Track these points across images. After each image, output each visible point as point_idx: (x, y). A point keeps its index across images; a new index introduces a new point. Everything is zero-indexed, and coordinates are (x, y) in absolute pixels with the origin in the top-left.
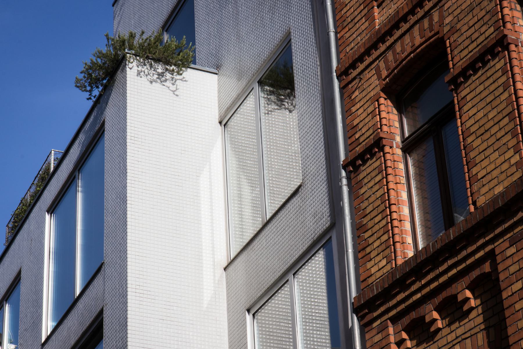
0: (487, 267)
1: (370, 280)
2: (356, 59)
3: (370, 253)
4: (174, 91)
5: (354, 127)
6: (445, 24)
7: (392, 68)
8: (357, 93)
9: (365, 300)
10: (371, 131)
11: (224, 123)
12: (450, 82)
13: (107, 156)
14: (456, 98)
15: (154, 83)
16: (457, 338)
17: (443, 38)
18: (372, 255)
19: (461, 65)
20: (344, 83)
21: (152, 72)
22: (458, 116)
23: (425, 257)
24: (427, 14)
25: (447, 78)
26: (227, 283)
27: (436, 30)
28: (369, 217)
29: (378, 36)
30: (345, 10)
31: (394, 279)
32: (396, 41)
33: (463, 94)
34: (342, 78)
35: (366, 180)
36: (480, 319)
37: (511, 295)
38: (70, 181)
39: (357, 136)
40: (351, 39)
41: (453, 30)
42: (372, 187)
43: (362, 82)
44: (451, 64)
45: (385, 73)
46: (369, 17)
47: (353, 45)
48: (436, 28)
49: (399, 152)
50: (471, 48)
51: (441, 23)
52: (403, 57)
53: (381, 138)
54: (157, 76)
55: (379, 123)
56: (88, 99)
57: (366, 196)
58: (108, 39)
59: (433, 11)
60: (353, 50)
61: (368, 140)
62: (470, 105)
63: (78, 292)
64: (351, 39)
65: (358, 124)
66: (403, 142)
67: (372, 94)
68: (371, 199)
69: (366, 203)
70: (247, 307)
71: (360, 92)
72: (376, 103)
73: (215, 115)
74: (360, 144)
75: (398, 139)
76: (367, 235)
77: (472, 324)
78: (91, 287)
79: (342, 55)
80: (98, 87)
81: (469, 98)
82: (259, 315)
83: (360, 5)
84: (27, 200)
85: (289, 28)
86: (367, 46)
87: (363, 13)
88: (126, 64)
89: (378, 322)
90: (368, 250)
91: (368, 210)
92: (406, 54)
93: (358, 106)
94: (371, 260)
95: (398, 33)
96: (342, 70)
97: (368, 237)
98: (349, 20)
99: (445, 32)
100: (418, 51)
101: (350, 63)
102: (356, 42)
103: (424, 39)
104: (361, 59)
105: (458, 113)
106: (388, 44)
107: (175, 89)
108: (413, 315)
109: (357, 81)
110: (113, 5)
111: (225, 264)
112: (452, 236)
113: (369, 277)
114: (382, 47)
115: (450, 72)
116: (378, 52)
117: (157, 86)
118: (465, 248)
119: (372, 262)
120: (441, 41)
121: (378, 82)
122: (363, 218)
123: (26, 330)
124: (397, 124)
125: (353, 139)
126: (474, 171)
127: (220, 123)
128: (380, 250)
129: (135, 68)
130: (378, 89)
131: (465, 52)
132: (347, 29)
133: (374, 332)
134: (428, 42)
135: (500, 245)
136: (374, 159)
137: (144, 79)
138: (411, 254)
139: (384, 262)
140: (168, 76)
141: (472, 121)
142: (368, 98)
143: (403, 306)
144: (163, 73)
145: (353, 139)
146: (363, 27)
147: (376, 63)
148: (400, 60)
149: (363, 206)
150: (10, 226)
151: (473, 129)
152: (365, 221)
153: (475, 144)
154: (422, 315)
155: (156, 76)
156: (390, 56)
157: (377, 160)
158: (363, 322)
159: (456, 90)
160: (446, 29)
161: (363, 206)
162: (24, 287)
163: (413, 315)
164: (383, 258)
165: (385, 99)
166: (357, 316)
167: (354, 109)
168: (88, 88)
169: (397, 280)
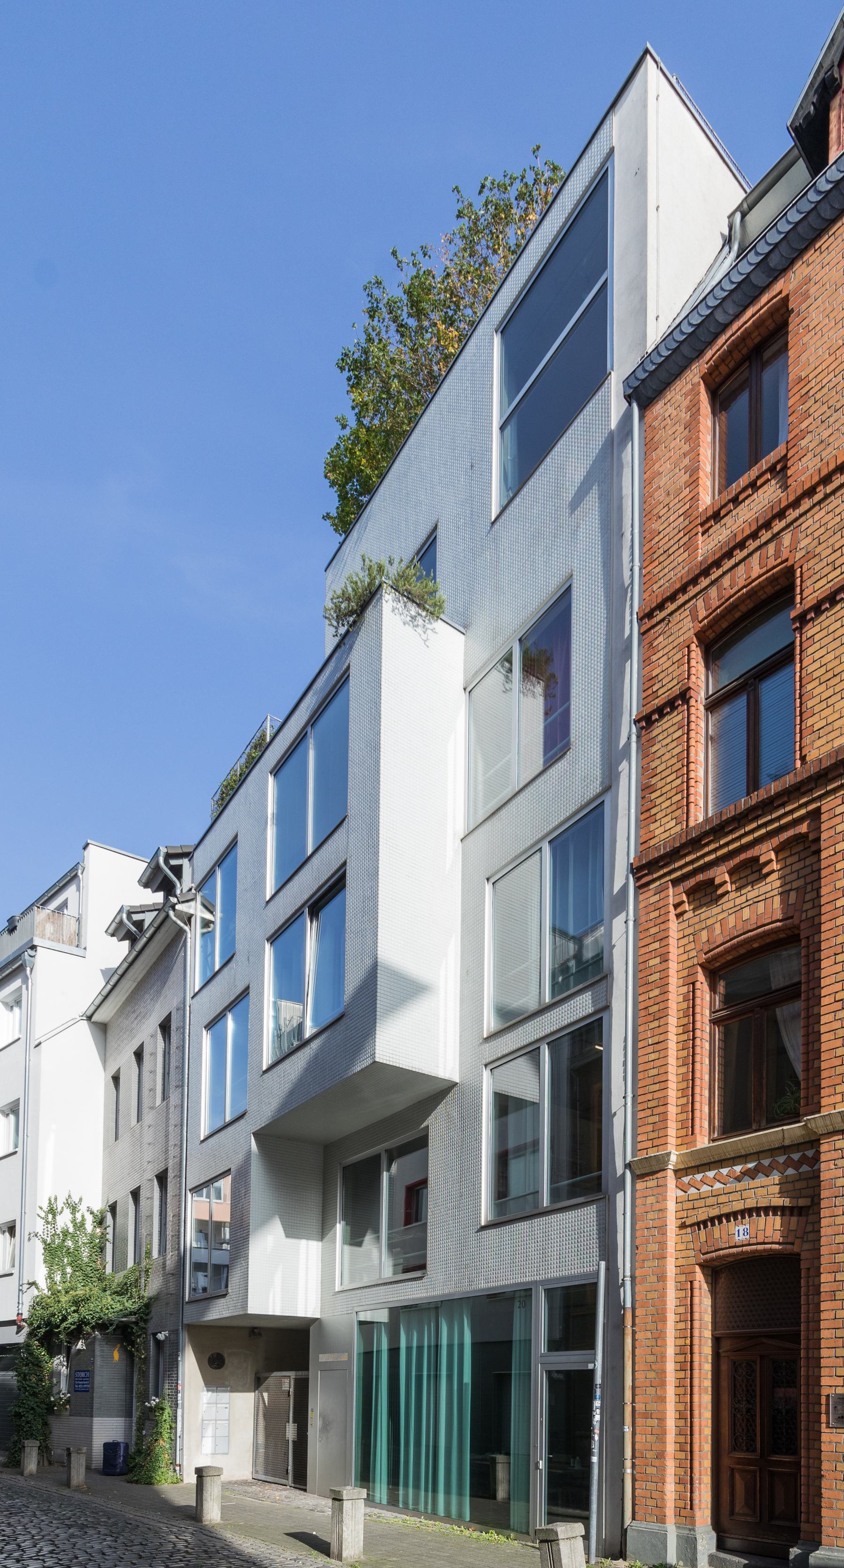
0: (803, 828)
1: (652, 842)
2: (668, 597)
3: (655, 814)
4: (425, 641)
5: (653, 678)
6: (798, 549)
7: (714, 607)
8: (661, 639)
9: (648, 860)
10: (675, 682)
11: (469, 690)
12: (794, 620)
13: (353, 705)
14: (798, 639)
15: (407, 625)
16: (747, 901)
17: (793, 566)
18: (658, 817)
19: (810, 600)
20: (643, 629)
21: (405, 612)
22: (798, 660)
23: (733, 814)
24: (775, 536)
25: (793, 614)
26: (463, 854)
27: (784, 558)
28: (658, 777)
29: (703, 568)
30: (657, 539)
31: (689, 838)
32: (724, 573)
33: (810, 634)
34: (644, 622)
35: (660, 737)
36: (778, 883)
37: (833, 855)
38: (300, 739)
39: (655, 688)
40: (661, 575)
41: (810, 555)
42: (667, 745)
43: (670, 625)
44: (798, 598)
45: (702, 613)
46: (690, 546)
47: (662, 582)
48: (785, 554)
49: (702, 708)
50: (830, 577)
51: (793, 549)
52: (732, 593)
53: (689, 688)
54: (410, 619)
55: (686, 673)
56: (334, 636)
57: (658, 754)
58: (364, 561)
59: (784, 533)
60: (662, 588)
61: (670, 692)
62: (817, 646)
63: (310, 851)
64: (661, 575)
65: (657, 675)
66: (706, 699)
67: (681, 639)
68: (664, 758)
69: (658, 762)
70: (487, 876)
71: (665, 637)
72: (686, 649)
73: (459, 680)
74: (658, 697)
75: (702, 694)
76: (653, 796)
77: (769, 888)
78: (330, 841)
79: (646, 595)
80: (343, 625)
81: (817, 638)
82: (498, 885)
83: (680, 531)
84: (236, 771)
85: (572, 570)
86: (685, 580)
87: (682, 542)
88: (381, 595)
89: (658, 883)
90: (653, 811)
91: (659, 770)
92: (736, 589)
93: (660, 654)
94: (656, 821)
95: (728, 564)
96: (646, 611)
97: (656, 798)
98: (661, 551)
99: (796, 559)
100: (753, 584)
101: (658, 602)
102: (667, 578)
103: (765, 569)
104: (672, 598)
105: (798, 657)
106: (713, 577)
107: (425, 639)
108: (701, 877)
109: (663, 625)
110: (326, 571)
111: (463, 836)
112: (773, 791)
113: (650, 839)
114: (704, 582)
115: (795, 607)
116: (698, 588)
117: (409, 629)
118: (783, 805)
119: (658, 824)
120: (790, 571)
121: (691, 625)
122: (652, 777)
123: (246, 890)
124: (703, 678)
125: (650, 692)
126: (810, 722)
127: (465, 689)
128: (669, 810)
129: (390, 602)
130: (692, 632)
131: (824, 581)
132: (656, 563)
133: (651, 893)
134: (771, 573)
135: (826, 804)
136: (675, 713)
137: (398, 617)
138: (701, 819)
139: (673, 823)
140: (420, 621)
141: (817, 665)
142: (675, 644)
143: (690, 868)
144: (416, 617)
145: (650, 692)
146: (680, 559)
147: (692, 603)
148: (726, 597)
149: (653, 765)
150: (216, 798)
151: (816, 675)
152: (653, 781)
153: (816, 692)
154: (711, 877)
155: (409, 618)
156: (713, 592)
157: (678, 714)
158: (637, 885)
159: (800, 629)
160: (799, 555)
161: (653, 765)
162: (242, 851)
163: (701, 877)
164: (672, 819)
165: (697, 646)
166: (633, 877)
167: (654, 658)
168: (335, 623)
169: (693, 839)
